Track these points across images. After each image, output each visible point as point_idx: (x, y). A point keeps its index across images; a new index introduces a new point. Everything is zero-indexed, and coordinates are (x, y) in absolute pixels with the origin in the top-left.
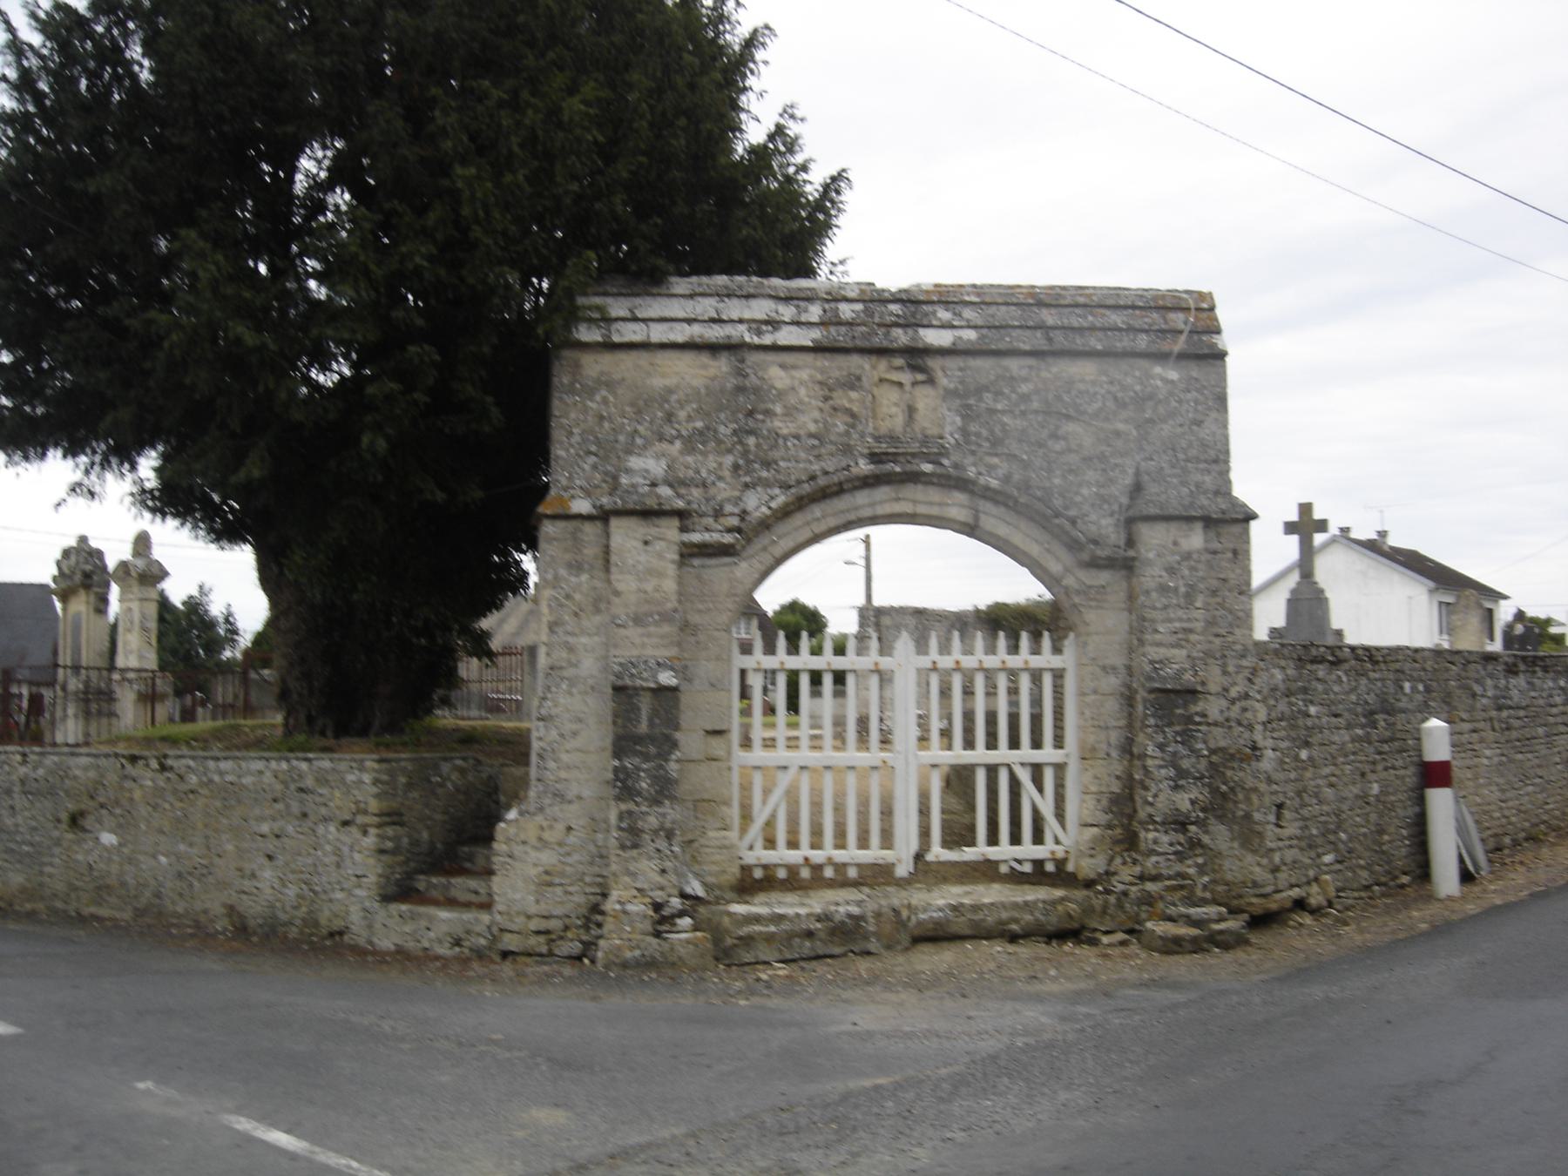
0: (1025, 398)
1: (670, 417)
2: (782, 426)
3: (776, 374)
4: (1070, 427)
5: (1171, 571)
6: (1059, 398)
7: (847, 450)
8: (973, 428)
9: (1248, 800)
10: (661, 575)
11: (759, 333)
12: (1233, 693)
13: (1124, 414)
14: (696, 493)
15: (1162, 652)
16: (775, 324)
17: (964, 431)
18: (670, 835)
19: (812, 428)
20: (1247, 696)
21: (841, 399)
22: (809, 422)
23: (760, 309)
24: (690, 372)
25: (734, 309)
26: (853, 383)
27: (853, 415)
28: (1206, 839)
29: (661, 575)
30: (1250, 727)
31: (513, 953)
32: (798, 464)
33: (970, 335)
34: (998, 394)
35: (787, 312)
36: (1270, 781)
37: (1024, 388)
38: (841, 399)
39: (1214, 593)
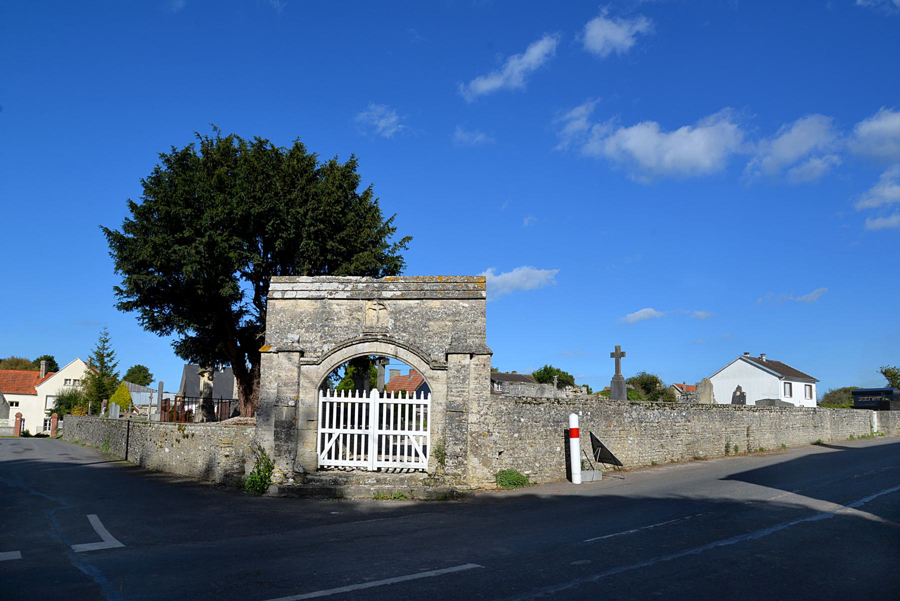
0: (416, 314)
1: (302, 321)
2: (337, 324)
3: (335, 306)
4: (431, 323)
5: (458, 371)
6: (426, 313)
7: (356, 331)
8: (398, 324)
9: (486, 449)
10: (293, 371)
11: (331, 294)
12: (482, 413)
13: (449, 318)
14: (309, 345)
15: (454, 398)
16: (336, 291)
17: (395, 325)
18: (290, 453)
19: (346, 324)
20: (487, 414)
21: (355, 315)
22: (345, 323)
23: (334, 286)
24: (307, 306)
25: (325, 286)
26: (360, 309)
27: (359, 320)
28: (465, 462)
29: (293, 371)
30: (488, 425)
31: (616, 462)
32: (342, 337)
33: (399, 293)
34: (407, 313)
35: (341, 287)
36: (495, 443)
37: (415, 311)
38: (355, 315)
39: (476, 379)
